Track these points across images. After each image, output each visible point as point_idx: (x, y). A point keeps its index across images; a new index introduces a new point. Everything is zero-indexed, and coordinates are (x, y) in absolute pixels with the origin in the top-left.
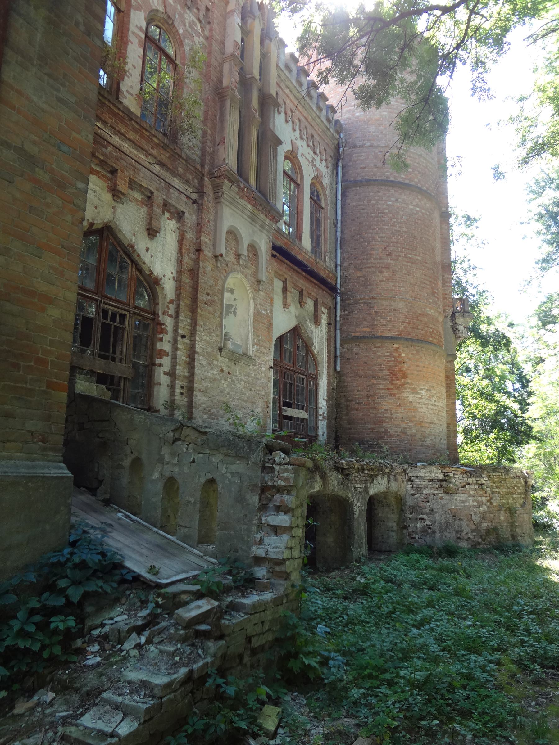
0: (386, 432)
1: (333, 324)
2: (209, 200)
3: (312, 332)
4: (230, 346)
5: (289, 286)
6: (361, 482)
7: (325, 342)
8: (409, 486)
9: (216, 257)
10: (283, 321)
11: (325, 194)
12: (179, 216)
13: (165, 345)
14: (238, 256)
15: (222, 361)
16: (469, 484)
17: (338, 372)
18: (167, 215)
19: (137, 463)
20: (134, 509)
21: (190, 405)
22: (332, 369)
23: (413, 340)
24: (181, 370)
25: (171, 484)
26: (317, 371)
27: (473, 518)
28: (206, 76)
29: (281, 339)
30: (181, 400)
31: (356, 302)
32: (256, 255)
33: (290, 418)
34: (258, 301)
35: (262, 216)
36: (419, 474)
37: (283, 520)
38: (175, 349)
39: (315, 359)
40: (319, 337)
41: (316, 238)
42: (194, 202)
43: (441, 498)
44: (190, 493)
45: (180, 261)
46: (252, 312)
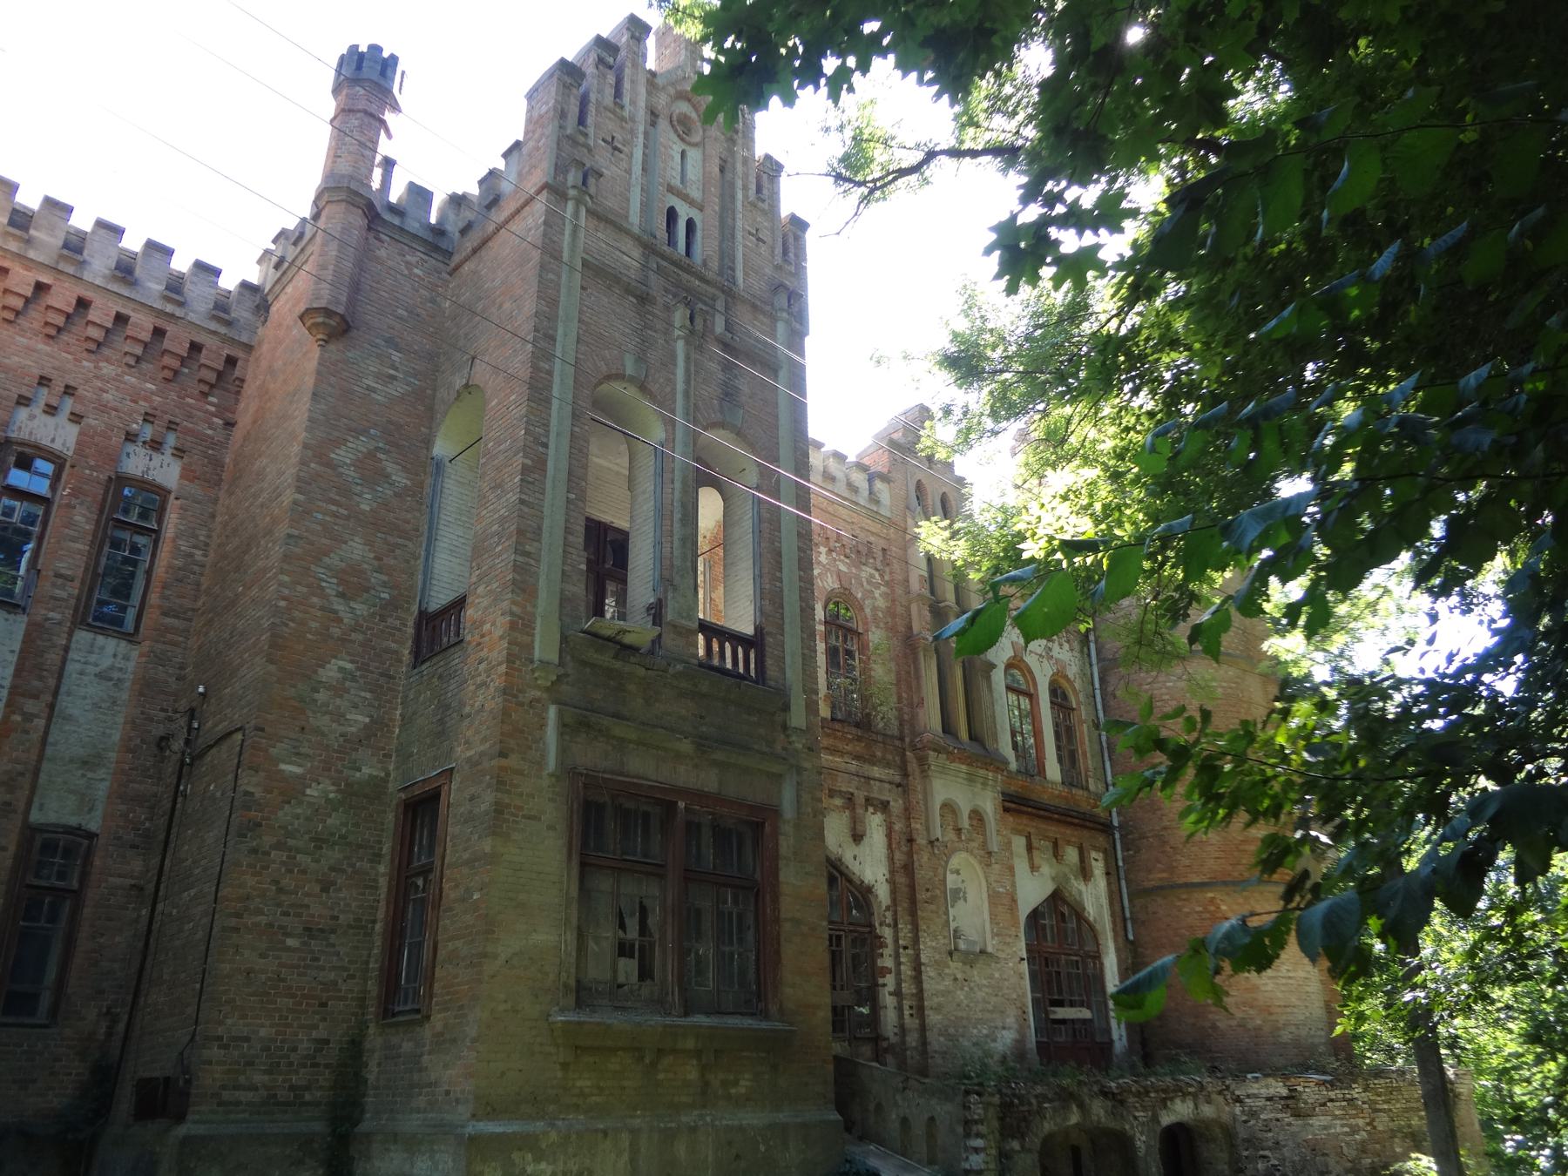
0: (1214, 1027)
1: (1114, 872)
2: (916, 782)
3: (1080, 893)
4: (962, 946)
5: (1035, 843)
6: (1144, 1109)
7: (1104, 901)
8: (1238, 1109)
9: (931, 843)
10: (1032, 890)
11: (1074, 689)
12: (884, 807)
13: (887, 962)
14: (959, 831)
15: (955, 967)
16: (1331, 1100)
17: (1132, 943)
18: (871, 809)
19: (879, 1107)
20: (880, 1142)
21: (923, 1028)
22: (1120, 940)
23: (1235, 883)
24: (908, 988)
25: (905, 1121)
26: (1098, 945)
27: (1345, 1150)
28: (892, 629)
29: (1035, 916)
30: (911, 1023)
31: (1143, 837)
32: (981, 820)
33: (1063, 1021)
34: (992, 879)
35: (982, 772)
36: (1251, 1091)
37: (979, 1143)
38: (898, 964)
39: (1092, 928)
40: (1094, 897)
41: (1068, 757)
42: (899, 785)
43: (1289, 1124)
44: (919, 1130)
45: (891, 859)
46: (985, 896)
